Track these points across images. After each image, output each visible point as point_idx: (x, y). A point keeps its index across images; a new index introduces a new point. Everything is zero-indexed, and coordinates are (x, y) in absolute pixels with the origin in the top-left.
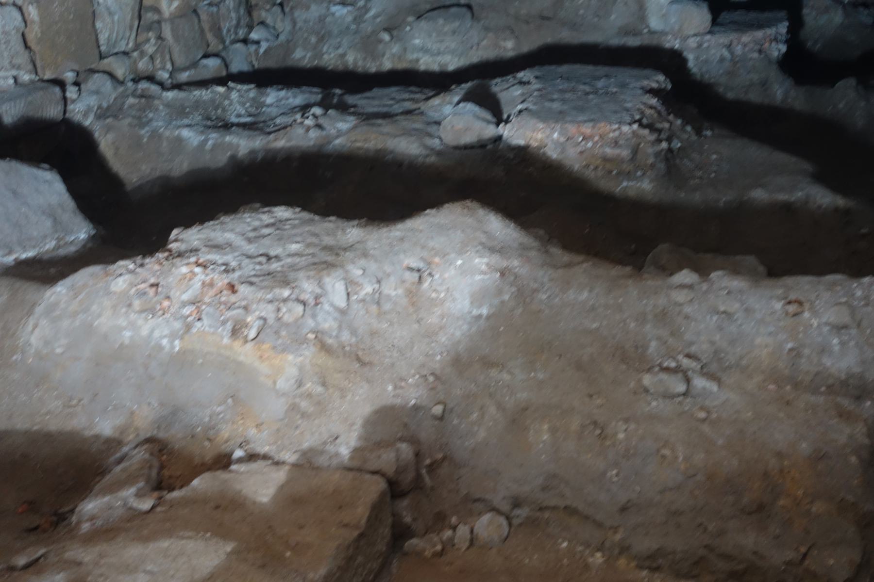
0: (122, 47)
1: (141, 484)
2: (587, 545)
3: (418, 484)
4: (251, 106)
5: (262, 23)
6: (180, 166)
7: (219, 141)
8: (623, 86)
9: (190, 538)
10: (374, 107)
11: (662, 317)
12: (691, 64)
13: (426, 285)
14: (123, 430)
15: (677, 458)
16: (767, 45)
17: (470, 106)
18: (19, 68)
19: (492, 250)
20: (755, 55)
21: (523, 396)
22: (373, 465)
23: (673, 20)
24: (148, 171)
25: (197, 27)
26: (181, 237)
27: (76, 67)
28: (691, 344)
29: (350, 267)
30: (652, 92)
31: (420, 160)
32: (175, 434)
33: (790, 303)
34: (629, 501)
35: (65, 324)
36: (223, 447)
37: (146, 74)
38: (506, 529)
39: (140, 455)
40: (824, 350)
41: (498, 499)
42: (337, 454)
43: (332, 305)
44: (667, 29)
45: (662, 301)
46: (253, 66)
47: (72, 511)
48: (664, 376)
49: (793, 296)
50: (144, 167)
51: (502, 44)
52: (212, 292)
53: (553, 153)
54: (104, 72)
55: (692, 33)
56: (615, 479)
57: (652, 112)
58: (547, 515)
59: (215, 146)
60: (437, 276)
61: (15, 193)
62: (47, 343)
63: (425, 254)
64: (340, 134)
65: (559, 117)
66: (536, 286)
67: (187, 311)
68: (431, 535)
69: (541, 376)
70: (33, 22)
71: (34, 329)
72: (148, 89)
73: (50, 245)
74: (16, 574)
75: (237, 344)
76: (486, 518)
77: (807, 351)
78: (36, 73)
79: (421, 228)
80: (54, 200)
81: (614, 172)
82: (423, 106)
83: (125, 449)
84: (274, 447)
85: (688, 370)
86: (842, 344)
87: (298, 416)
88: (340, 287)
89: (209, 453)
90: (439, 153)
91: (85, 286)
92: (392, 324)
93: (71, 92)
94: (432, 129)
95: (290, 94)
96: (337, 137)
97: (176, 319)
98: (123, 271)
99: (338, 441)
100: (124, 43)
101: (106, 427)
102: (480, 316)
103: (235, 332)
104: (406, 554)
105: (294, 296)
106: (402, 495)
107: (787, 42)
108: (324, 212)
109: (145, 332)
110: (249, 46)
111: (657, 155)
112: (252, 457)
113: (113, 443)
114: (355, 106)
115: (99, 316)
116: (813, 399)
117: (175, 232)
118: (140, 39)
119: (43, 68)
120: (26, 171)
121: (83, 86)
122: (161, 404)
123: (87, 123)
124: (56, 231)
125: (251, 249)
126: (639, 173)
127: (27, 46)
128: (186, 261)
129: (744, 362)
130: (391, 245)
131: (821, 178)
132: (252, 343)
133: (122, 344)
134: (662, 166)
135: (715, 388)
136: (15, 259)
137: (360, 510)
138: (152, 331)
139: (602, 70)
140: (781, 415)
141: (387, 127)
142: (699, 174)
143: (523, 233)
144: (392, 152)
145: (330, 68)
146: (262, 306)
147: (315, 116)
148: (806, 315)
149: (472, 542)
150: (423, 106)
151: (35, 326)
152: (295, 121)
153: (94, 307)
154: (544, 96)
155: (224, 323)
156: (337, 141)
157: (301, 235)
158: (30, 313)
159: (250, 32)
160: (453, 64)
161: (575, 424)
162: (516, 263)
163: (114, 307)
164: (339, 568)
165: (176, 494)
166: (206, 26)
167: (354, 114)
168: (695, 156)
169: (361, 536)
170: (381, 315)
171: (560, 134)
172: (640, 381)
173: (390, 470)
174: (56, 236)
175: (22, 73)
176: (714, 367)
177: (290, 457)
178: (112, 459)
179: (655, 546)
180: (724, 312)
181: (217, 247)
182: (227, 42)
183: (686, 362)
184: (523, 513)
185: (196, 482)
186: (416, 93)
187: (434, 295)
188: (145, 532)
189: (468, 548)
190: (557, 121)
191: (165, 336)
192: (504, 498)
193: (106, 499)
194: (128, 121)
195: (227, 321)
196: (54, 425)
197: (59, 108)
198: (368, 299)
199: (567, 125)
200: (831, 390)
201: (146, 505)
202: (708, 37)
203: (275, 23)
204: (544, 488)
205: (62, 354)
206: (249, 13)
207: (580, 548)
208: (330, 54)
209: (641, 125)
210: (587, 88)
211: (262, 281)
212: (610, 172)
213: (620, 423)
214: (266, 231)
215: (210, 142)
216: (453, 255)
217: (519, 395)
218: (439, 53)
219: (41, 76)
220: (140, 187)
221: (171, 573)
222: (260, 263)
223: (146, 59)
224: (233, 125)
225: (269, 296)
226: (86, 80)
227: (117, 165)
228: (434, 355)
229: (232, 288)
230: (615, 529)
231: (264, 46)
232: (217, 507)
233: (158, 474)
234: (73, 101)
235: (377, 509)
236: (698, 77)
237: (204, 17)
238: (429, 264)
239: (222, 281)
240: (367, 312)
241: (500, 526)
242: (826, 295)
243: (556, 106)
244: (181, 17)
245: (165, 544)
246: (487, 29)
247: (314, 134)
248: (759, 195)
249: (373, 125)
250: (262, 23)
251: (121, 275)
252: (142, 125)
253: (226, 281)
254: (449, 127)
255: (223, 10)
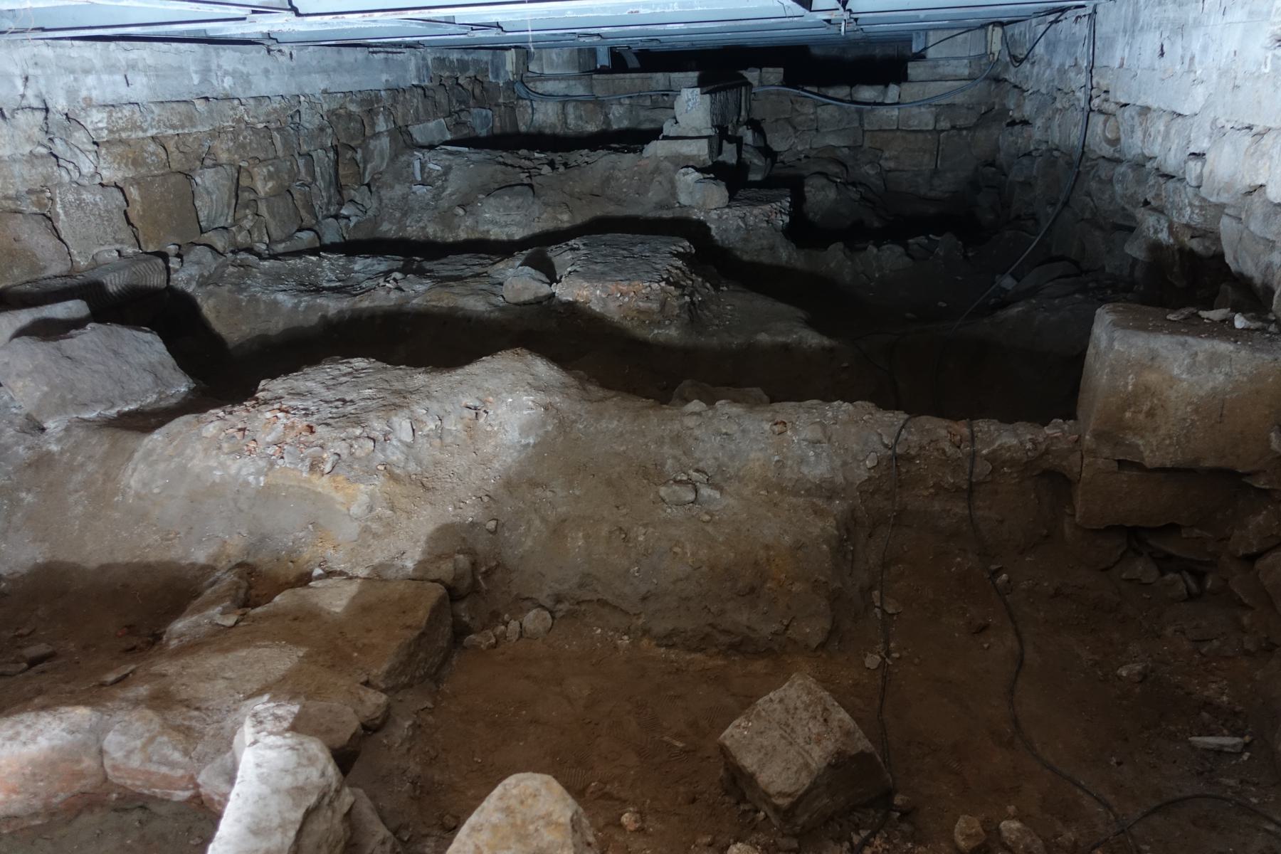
0: (221, 222)
1: (227, 603)
2: (616, 630)
3: (474, 589)
4: (341, 273)
5: (352, 201)
6: (276, 325)
7: (311, 303)
8: (655, 251)
9: (266, 646)
10: (447, 271)
11: (677, 439)
12: (713, 233)
13: (482, 420)
14: (216, 558)
15: (686, 553)
16: (773, 217)
17: (527, 269)
18: (122, 242)
19: (538, 389)
20: (765, 225)
21: (562, 510)
22: (434, 574)
23: (698, 197)
24: (248, 331)
25: (291, 205)
26: (267, 387)
27: (178, 241)
28: (700, 460)
29: (415, 408)
30: (678, 255)
31: (486, 315)
32: (263, 559)
33: (776, 424)
34: (648, 592)
35: (161, 467)
36: (305, 566)
37: (244, 247)
38: (550, 621)
39: (230, 578)
40: (802, 460)
41: (543, 598)
42: (404, 567)
43: (400, 441)
44: (693, 204)
45: (677, 426)
46: (344, 238)
47: (165, 632)
48: (676, 488)
49: (778, 419)
50: (244, 328)
51: (559, 217)
52: (293, 434)
53: (597, 308)
54: (205, 245)
55: (714, 207)
56: (637, 574)
57: (678, 271)
58: (583, 607)
59: (307, 308)
60: (491, 413)
61: (115, 353)
62: (145, 485)
63: (480, 394)
64: (417, 294)
65: (601, 277)
66: (574, 417)
67: (271, 451)
68: (487, 631)
69: (577, 493)
70: (135, 200)
71: (133, 473)
72: (248, 258)
73: (152, 398)
74: (104, 688)
75: (315, 478)
76: (532, 614)
77: (790, 462)
78: (140, 248)
79: (478, 372)
80: (154, 358)
81: (647, 322)
82: (490, 270)
83: (218, 574)
84: (349, 565)
85: (697, 482)
86: (817, 455)
87: (371, 537)
88: (406, 425)
89: (292, 572)
90: (502, 309)
91: (180, 433)
92: (452, 454)
93: (174, 263)
94: (497, 289)
95: (375, 262)
96: (415, 297)
97: (261, 458)
98: (214, 418)
99: (404, 557)
100: (223, 219)
101: (200, 556)
102: (528, 444)
103: (313, 467)
104: (465, 648)
105: (365, 434)
106: (461, 598)
107: (789, 214)
108: (395, 363)
109: (233, 471)
110: (340, 220)
111: (681, 307)
112: (329, 574)
113: (208, 569)
114: (432, 271)
115: (192, 458)
116: (794, 500)
117: (263, 382)
118: (238, 216)
119: (146, 242)
120: (126, 332)
121: (185, 258)
122: (251, 533)
123: (190, 290)
124: (157, 385)
125: (330, 395)
126: (667, 322)
127: (129, 223)
128: (271, 408)
129: (741, 474)
130: (451, 388)
131: (812, 324)
132: (329, 475)
133: (214, 482)
134: (686, 316)
135: (718, 496)
136: (118, 412)
137: (421, 613)
138: (240, 469)
139: (639, 237)
140: (770, 514)
141: (457, 288)
142: (717, 322)
143: (564, 373)
144: (462, 309)
145: (414, 238)
146: (336, 444)
147: (395, 279)
148: (789, 433)
149: (521, 635)
150: (490, 270)
151: (134, 470)
152: (378, 284)
153: (188, 451)
154: (590, 260)
155: (303, 460)
156: (414, 301)
157: (374, 382)
158: (129, 459)
159: (341, 208)
160: (518, 234)
161: (605, 530)
162: (558, 400)
163: (206, 450)
164: (401, 663)
165: (259, 610)
166: (299, 204)
167: (429, 277)
168: (714, 307)
169: (423, 634)
170: (443, 447)
171: (602, 291)
172: (657, 492)
173: (448, 578)
174: (157, 390)
175: (126, 246)
176: (718, 478)
177: (362, 572)
178: (206, 584)
179: (670, 627)
180: (726, 434)
181: (300, 395)
182: (320, 218)
183: (695, 475)
184: (564, 607)
185: (277, 599)
186: (484, 259)
187: (489, 429)
188: (226, 644)
189: (517, 640)
190: (599, 280)
191: (251, 474)
192: (549, 595)
193: (194, 618)
194: (228, 287)
195: (306, 457)
196: (153, 557)
197: (162, 277)
198: (431, 433)
199: (607, 284)
200: (809, 492)
201: (230, 621)
202: (727, 210)
203: (363, 200)
204: (581, 586)
205: (160, 493)
206: (340, 193)
207: (610, 634)
208: (412, 227)
209: (668, 282)
210: (625, 252)
211: (337, 422)
212: (644, 322)
213: (641, 528)
214: (344, 379)
215: (303, 304)
216: (504, 395)
217: (559, 510)
218: (506, 225)
219: (145, 250)
220: (241, 346)
221: (247, 678)
222: (337, 407)
223: (244, 233)
224: (324, 288)
225: (343, 435)
226: (188, 253)
227: (219, 326)
228: (490, 479)
229: (311, 429)
230: (638, 615)
231: (354, 220)
232: (295, 619)
233: (246, 594)
234: (176, 271)
235: (436, 611)
236: (720, 243)
237: (297, 196)
238: (484, 402)
239: (301, 423)
240: (431, 445)
241: (545, 619)
242: (804, 416)
243: (598, 268)
244: (274, 196)
245: (243, 653)
246: (546, 204)
247: (394, 295)
248: (763, 338)
249: (446, 286)
250: (352, 201)
251: (212, 422)
252: (241, 290)
253: (306, 423)
254: (510, 288)
255: (315, 190)
